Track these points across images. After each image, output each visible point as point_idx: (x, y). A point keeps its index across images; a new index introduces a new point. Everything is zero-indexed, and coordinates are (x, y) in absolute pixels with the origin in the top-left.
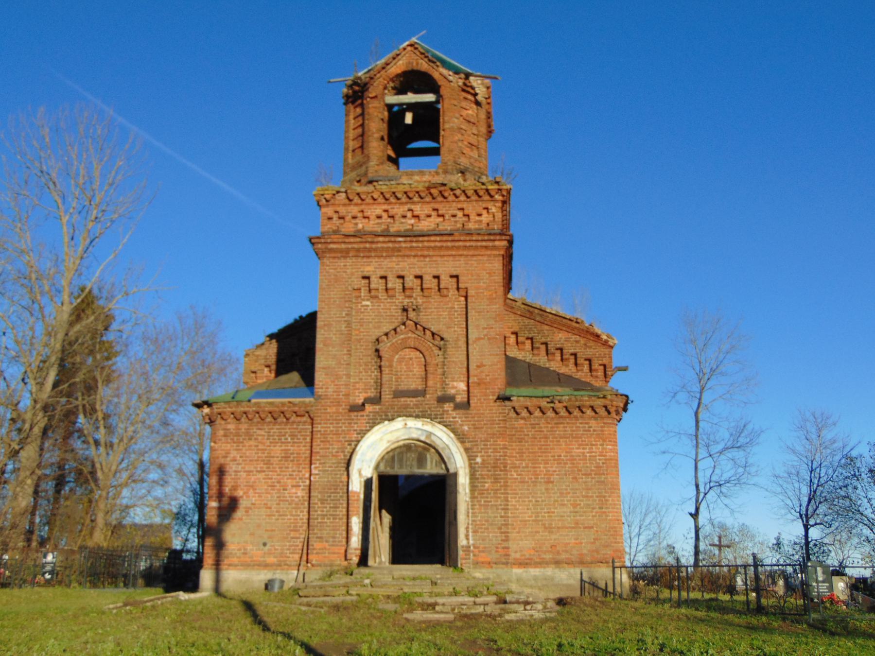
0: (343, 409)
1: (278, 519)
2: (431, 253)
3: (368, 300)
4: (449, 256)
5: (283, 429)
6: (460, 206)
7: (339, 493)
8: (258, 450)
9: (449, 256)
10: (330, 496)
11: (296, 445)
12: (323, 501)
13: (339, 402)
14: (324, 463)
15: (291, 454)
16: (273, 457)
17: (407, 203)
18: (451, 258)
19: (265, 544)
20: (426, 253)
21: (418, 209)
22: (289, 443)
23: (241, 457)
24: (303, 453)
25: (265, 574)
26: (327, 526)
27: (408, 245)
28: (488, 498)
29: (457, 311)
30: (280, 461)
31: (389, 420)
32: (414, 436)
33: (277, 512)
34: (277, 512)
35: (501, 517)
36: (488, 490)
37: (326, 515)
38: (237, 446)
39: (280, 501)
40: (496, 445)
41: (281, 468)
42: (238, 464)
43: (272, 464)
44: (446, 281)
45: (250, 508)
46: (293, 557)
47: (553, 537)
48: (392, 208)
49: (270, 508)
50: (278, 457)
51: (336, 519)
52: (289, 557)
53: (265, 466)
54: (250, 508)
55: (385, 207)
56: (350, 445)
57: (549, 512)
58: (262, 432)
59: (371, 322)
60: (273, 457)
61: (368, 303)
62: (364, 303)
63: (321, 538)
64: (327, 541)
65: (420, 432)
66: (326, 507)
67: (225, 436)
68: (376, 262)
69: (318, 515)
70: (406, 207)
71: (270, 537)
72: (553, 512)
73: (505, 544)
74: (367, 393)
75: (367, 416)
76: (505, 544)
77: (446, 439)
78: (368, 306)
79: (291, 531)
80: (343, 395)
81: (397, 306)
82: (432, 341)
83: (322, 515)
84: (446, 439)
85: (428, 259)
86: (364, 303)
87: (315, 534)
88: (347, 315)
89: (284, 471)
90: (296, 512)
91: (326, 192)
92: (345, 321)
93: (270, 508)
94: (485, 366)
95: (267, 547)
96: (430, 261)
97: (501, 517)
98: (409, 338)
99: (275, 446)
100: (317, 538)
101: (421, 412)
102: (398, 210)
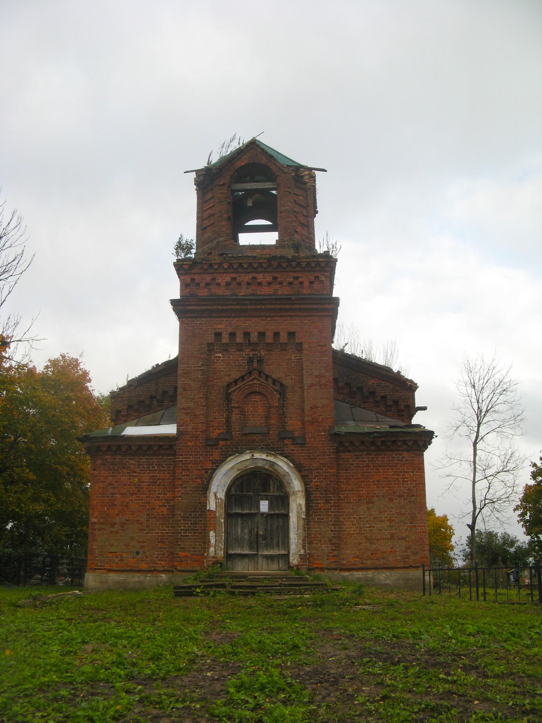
0: (201, 443)
1: (148, 533)
2: (272, 314)
3: (219, 353)
4: (287, 316)
5: (151, 459)
6: (295, 275)
7: (198, 512)
8: (130, 476)
9: (287, 316)
10: (191, 515)
11: (162, 472)
12: (184, 518)
13: (197, 437)
14: (185, 487)
15: (158, 479)
16: (143, 482)
17: (251, 272)
18: (289, 318)
19: (138, 553)
20: (268, 314)
21: (260, 277)
22: (156, 470)
23: (116, 482)
24: (168, 479)
25: (139, 577)
26: (189, 539)
27: (253, 307)
28: (320, 515)
29: (294, 362)
30: (148, 485)
31: (239, 453)
32: (260, 465)
33: (147, 527)
34: (147, 527)
35: (331, 531)
36: (320, 509)
37: (188, 530)
38: (113, 473)
39: (150, 518)
40: (328, 472)
41: (150, 491)
42: (116, 488)
43: (142, 488)
44: (284, 338)
45: (125, 524)
46: (161, 564)
47: (373, 546)
48: (238, 276)
49: (141, 524)
50: (147, 482)
51: (196, 533)
52: (158, 564)
53: (136, 490)
54: (125, 524)
55: (233, 275)
56: (207, 472)
57: (369, 527)
58: (131, 462)
59: (223, 371)
60: (143, 482)
61: (220, 355)
62: (216, 355)
63: (184, 548)
64: (189, 551)
65: (264, 462)
66: (188, 524)
67: (103, 464)
68: (226, 321)
69: (181, 530)
70: (251, 276)
71: (142, 547)
72: (374, 527)
73: (336, 553)
74: (221, 430)
75: (220, 448)
76: (336, 553)
77: (285, 468)
78: (220, 357)
79: (159, 542)
80: (200, 431)
81: (244, 357)
82: (272, 385)
83: (186, 530)
84: (285, 468)
85: (269, 319)
86: (216, 355)
87: (179, 545)
88: (202, 365)
89: (152, 494)
90: (163, 527)
91: (185, 263)
92: (201, 370)
93: (141, 524)
94: (317, 407)
95: (139, 556)
96: (270, 320)
97: (331, 531)
98: (254, 384)
99: (144, 473)
100: (181, 548)
101: (265, 445)
102: (247, 278)
